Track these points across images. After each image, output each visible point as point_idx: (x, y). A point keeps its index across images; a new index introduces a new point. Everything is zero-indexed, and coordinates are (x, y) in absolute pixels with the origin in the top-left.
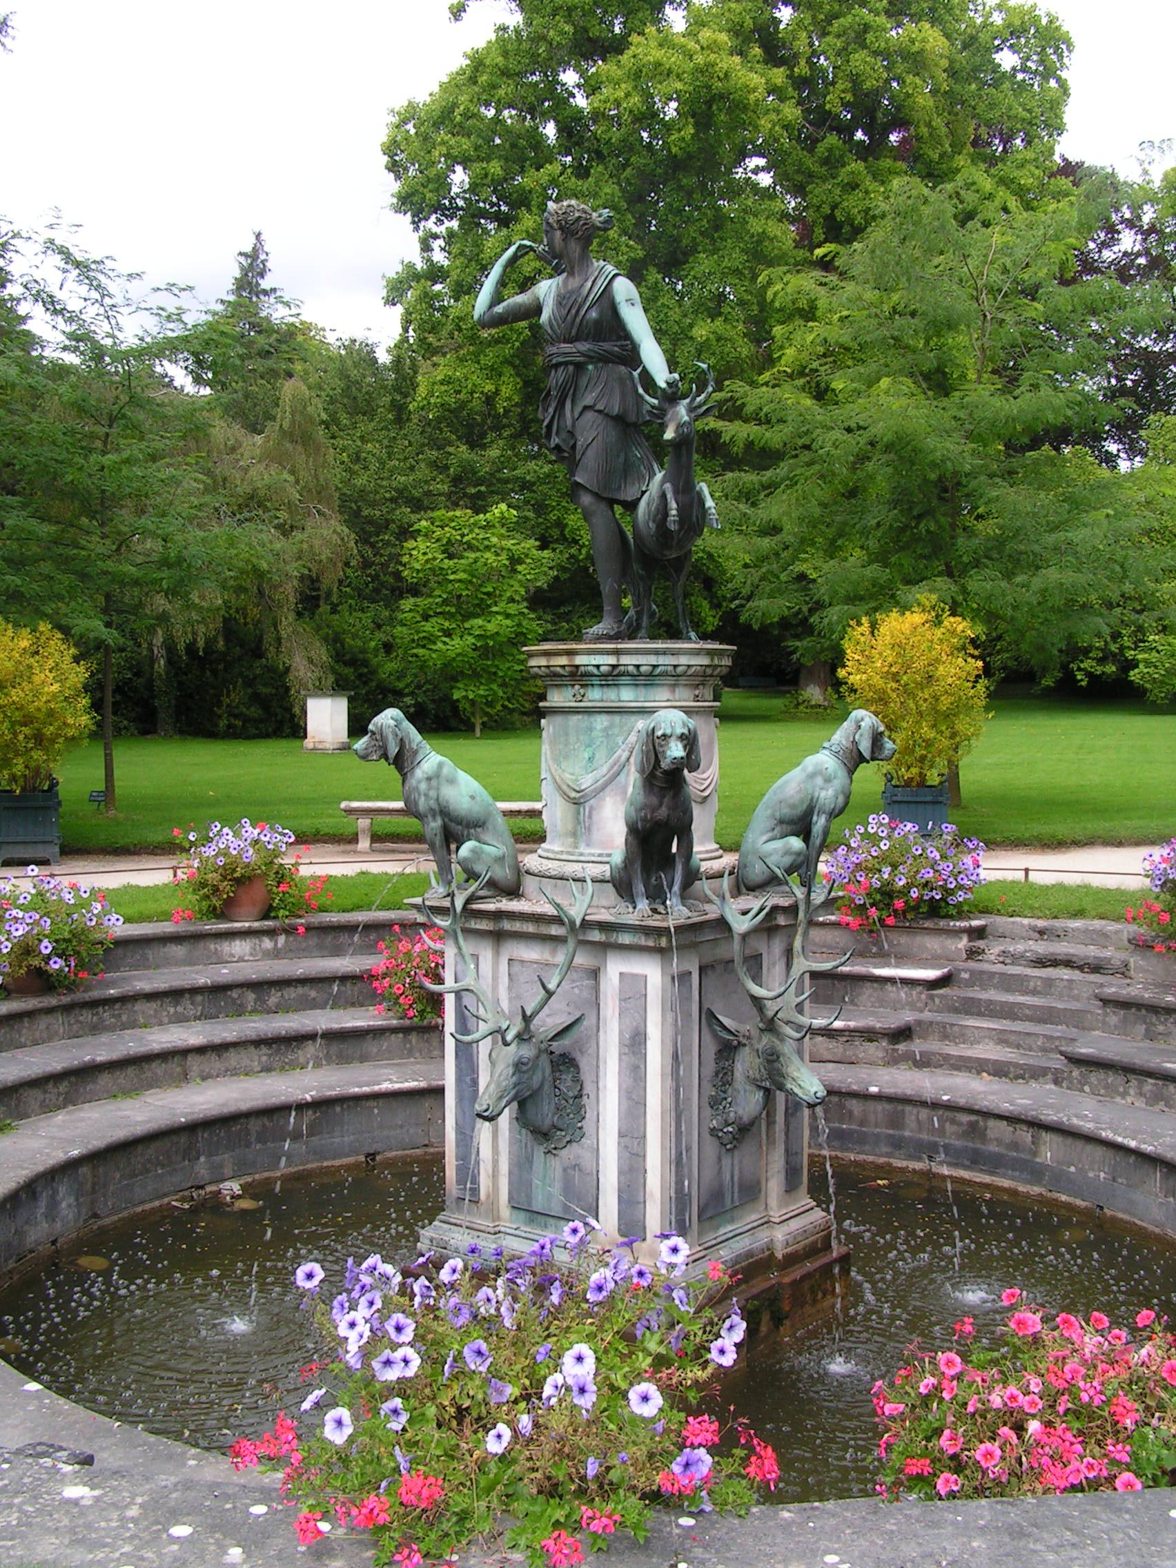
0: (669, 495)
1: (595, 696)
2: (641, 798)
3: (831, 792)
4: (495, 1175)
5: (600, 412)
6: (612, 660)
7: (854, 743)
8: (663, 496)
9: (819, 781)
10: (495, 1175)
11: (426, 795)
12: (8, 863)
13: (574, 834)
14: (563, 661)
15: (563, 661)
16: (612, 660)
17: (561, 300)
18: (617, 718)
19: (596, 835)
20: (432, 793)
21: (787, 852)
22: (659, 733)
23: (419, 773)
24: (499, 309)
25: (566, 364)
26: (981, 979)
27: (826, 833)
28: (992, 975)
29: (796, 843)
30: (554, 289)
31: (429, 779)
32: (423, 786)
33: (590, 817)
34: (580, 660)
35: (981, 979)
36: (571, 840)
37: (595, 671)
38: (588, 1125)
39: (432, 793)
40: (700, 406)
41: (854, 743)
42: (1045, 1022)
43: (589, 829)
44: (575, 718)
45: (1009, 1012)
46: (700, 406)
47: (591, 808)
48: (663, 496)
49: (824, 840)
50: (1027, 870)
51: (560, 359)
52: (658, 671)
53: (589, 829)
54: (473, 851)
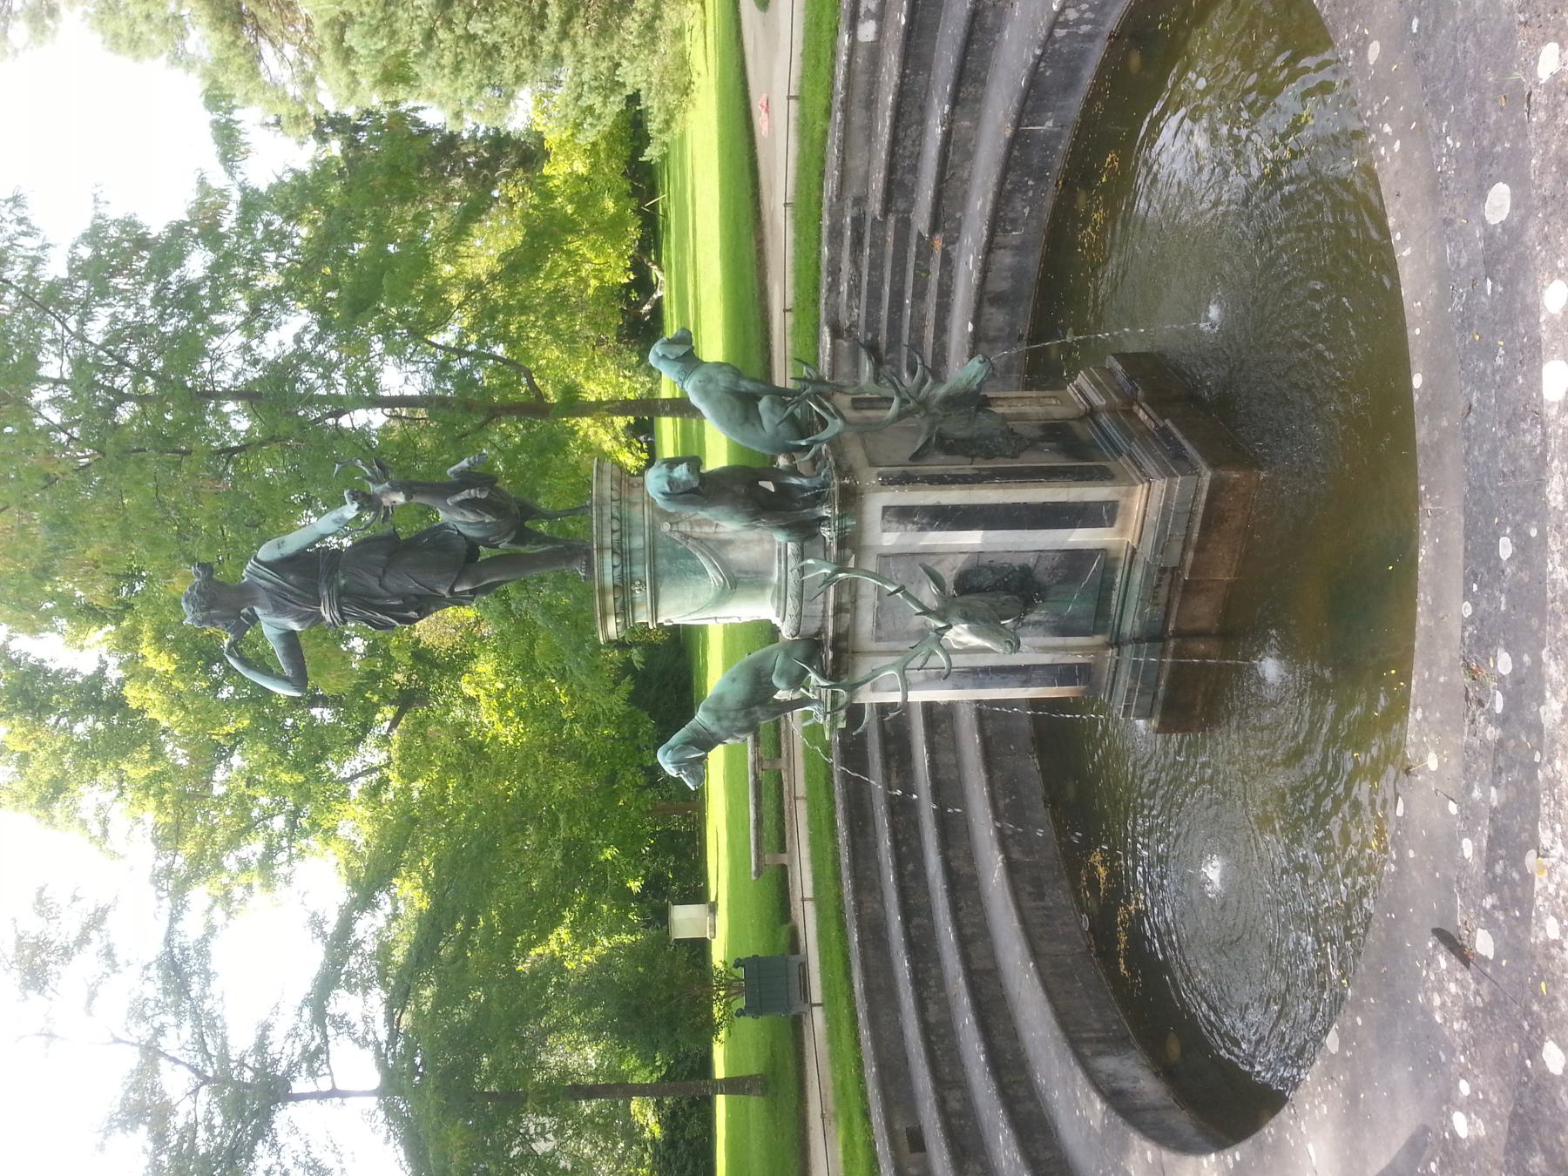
0: (458, 498)
2: (726, 509)
3: (720, 377)
4: (1065, 649)
5: (384, 572)
7: (678, 359)
8: (461, 504)
9: (711, 387)
10: (1065, 649)
11: (735, 720)
14: (610, 599)
15: (610, 599)
17: (279, 609)
20: (732, 715)
21: (772, 410)
22: (667, 489)
23: (714, 729)
24: (288, 672)
26: (872, 324)
27: (753, 380)
28: (868, 314)
29: (763, 404)
30: (269, 619)
31: (719, 719)
34: (609, 581)
35: (872, 324)
38: (1017, 561)
39: (732, 715)
41: (678, 359)
45: (897, 296)
47: (739, 571)
48: (461, 504)
49: (761, 381)
52: (617, 514)
54: (780, 676)
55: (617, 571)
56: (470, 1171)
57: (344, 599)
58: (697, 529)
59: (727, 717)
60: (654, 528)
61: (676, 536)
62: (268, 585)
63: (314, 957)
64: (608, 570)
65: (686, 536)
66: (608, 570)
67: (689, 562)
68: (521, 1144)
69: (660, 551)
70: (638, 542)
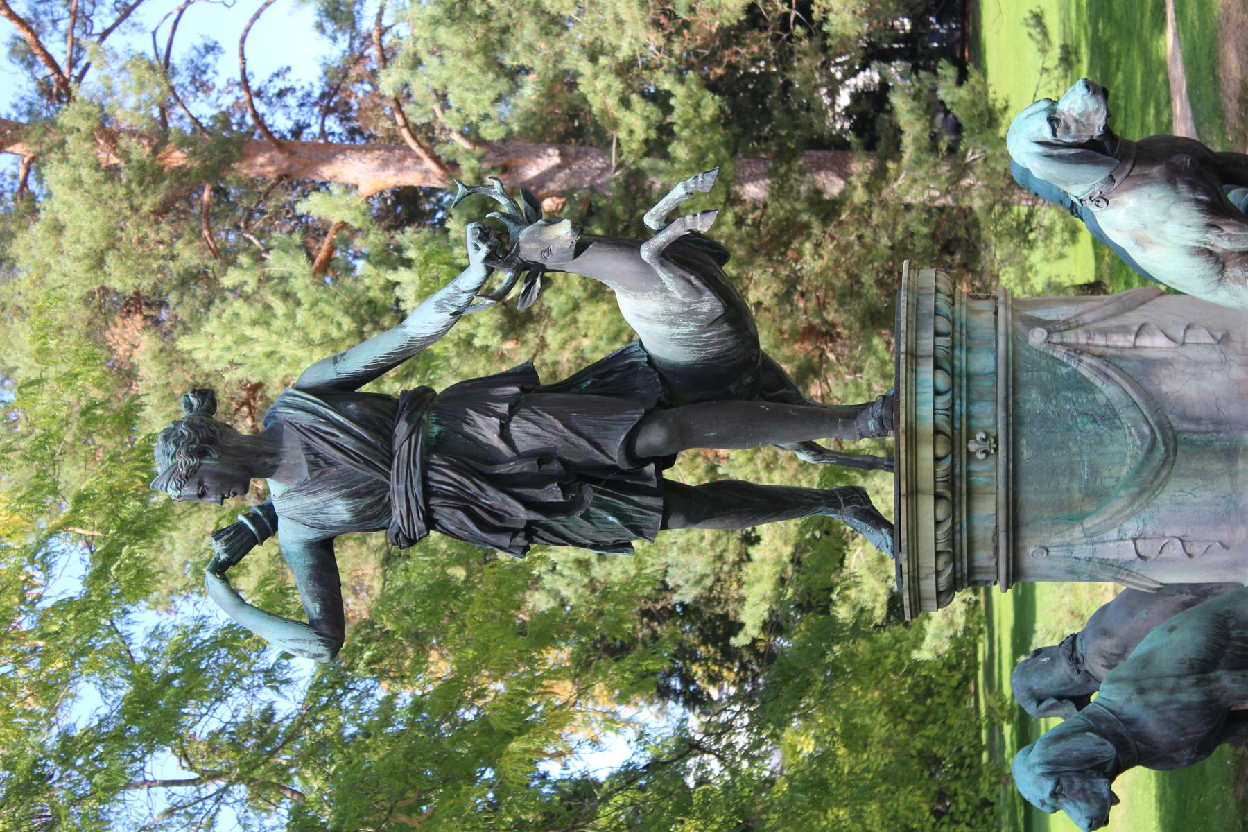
14: (926, 453)
31: (1141, 691)
39: (1170, 683)
47: (1184, 417)
55: (943, 401)
56: (3, 174)
57: (435, 459)
58: (1099, 340)
59: (1158, 687)
60: (1015, 341)
61: (1059, 353)
62: (305, 419)
63: (218, 818)
64: (926, 395)
65: (1078, 351)
66: (926, 395)
67: (1083, 398)
68: (940, 175)
69: (1024, 377)
70: (983, 362)
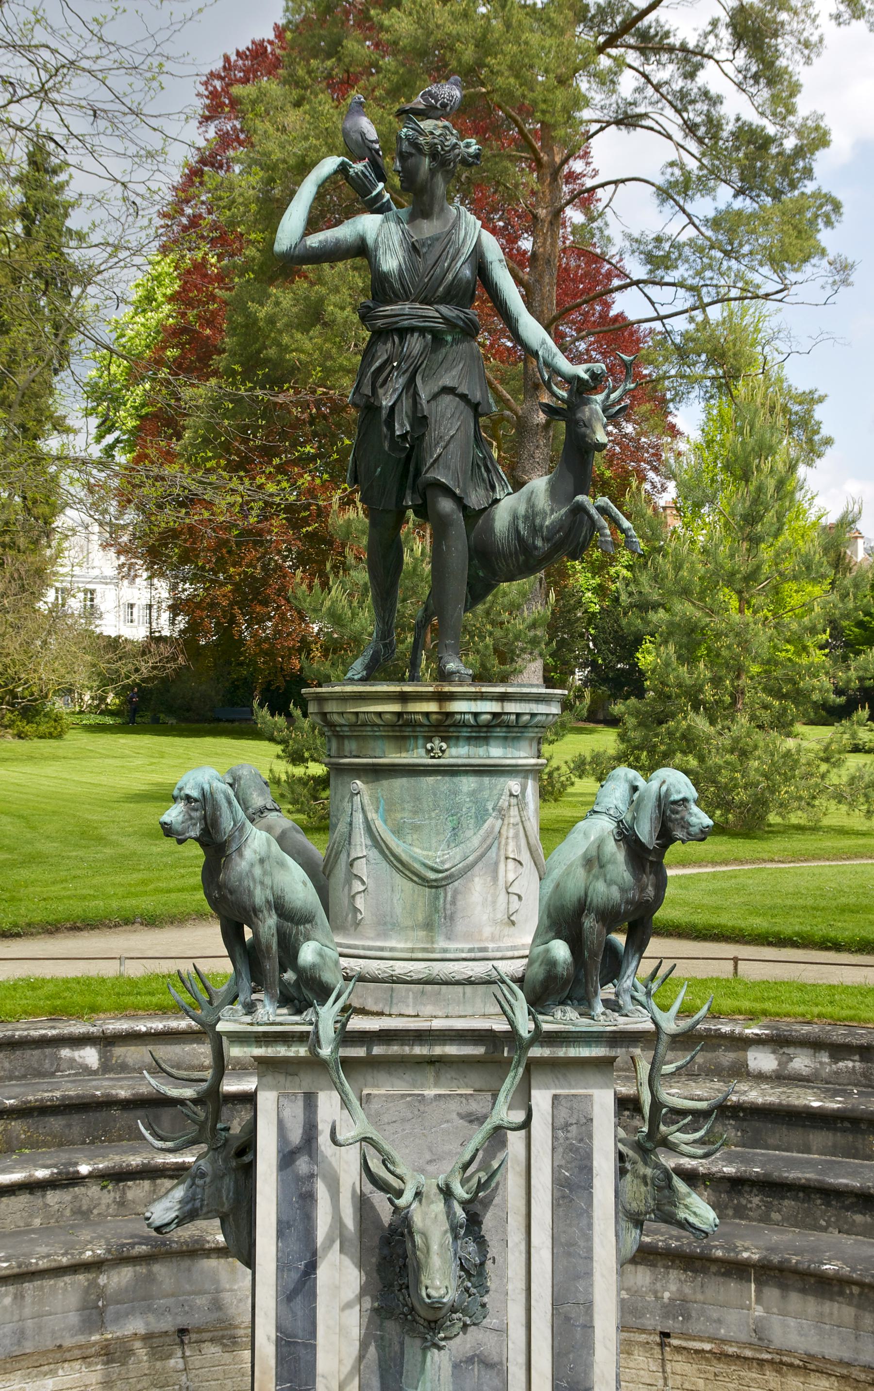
1: (459, 753)
6: (494, 707)
11: (262, 883)
12: (866, 909)
13: (429, 926)
16: (494, 707)
18: (486, 780)
19: (460, 926)
25: (422, 331)
31: (262, 861)
32: (257, 871)
33: (454, 902)
36: (422, 933)
37: (378, 721)
39: (268, 881)
40: (613, 405)
42: (588, 1156)
43: (452, 918)
44: (430, 780)
46: (613, 405)
47: (456, 892)
50: (736, 960)
51: (415, 322)
53: (451, 918)
